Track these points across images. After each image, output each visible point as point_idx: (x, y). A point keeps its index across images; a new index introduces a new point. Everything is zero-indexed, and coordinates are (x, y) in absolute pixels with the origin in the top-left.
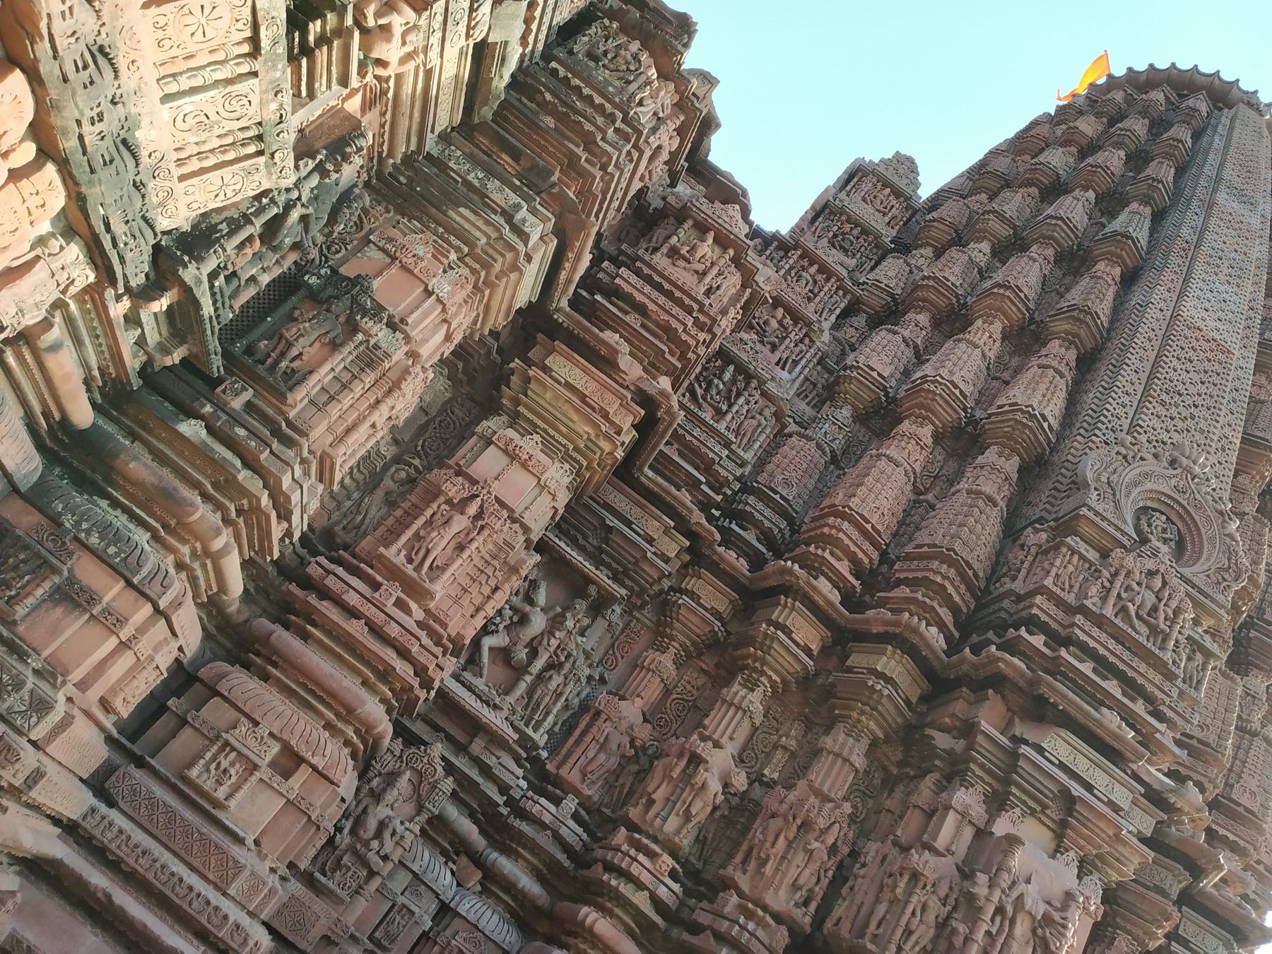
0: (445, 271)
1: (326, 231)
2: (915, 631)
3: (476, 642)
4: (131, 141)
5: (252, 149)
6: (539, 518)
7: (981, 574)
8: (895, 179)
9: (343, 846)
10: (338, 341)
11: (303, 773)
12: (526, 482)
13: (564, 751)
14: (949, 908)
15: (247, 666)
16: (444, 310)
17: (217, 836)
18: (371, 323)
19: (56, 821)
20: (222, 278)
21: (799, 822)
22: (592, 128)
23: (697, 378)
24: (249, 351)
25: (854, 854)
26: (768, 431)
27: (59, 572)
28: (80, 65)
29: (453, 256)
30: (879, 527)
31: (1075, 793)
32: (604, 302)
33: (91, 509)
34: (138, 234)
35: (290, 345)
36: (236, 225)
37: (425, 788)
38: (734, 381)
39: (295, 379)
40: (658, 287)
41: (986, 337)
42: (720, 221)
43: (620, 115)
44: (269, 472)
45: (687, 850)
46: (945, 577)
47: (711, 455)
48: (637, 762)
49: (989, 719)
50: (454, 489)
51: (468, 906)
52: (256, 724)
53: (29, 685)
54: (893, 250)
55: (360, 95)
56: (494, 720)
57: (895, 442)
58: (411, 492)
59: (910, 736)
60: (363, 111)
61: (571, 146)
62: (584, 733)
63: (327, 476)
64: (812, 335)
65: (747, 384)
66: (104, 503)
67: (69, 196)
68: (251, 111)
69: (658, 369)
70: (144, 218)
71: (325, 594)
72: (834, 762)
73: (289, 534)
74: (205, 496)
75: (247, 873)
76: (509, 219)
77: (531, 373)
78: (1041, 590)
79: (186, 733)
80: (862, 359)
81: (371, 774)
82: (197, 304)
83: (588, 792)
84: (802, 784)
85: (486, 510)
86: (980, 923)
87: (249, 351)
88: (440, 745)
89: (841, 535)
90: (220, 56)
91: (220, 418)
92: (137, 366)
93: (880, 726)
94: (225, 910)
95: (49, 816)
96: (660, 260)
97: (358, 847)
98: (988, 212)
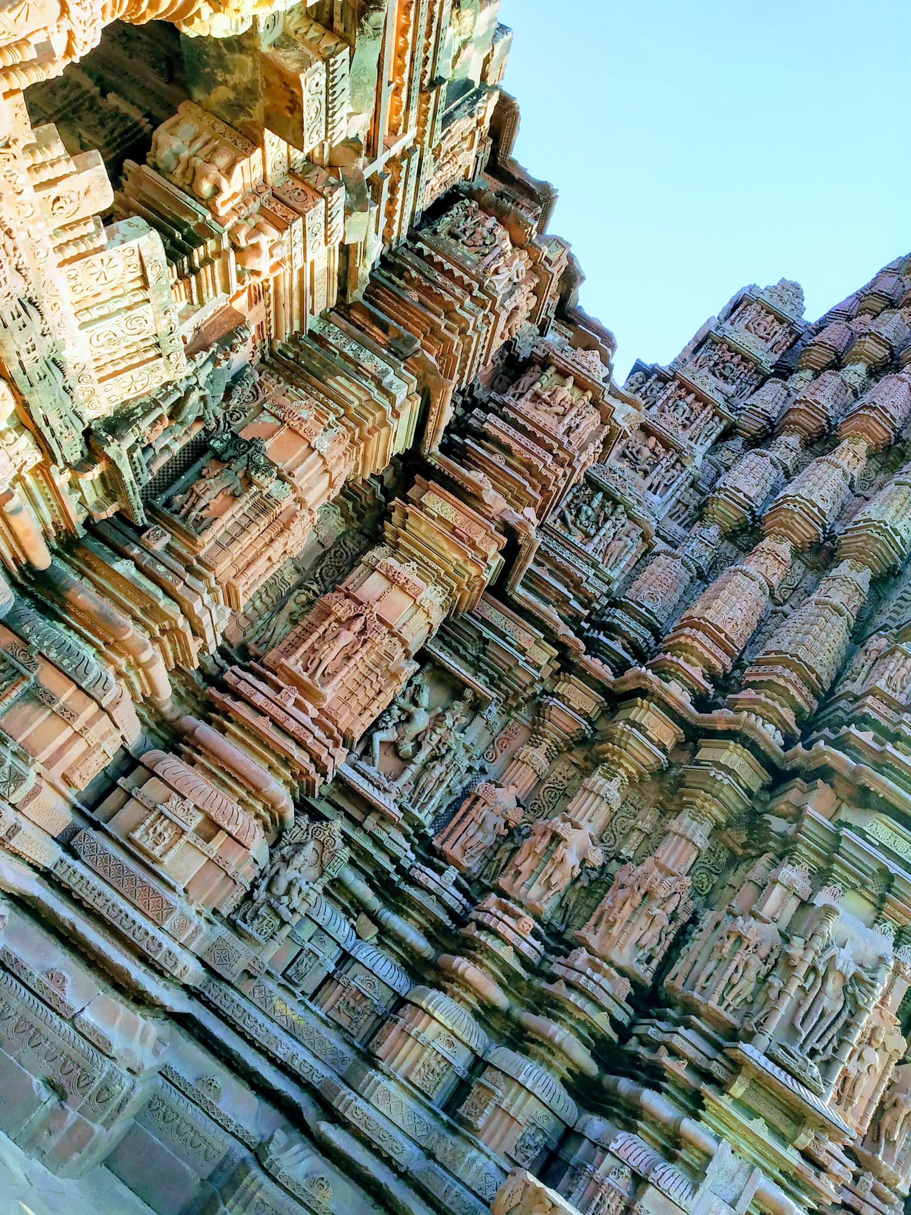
0: (325, 430)
1: (224, 405)
2: (753, 728)
3: (367, 737)
4: (58, 360)
5: (152, 353)
6: (416, 634)
7: (824, 677)
8: (779, 306)
9: (260, 901)
10: (237, 493)
11: (221, 838)
12: (407, 602)
13: (448, 830)
14: (769, 966)
15: (179, 753)
16: (325, 463)
17: (155, 884)
18: (263, 477)
19: (36, 869)
20: (139, 451)
21: (643, 891)
22: (452, 299)
23: (568, 506)
24: (168, 503)
25: (694, 920)
26: (634, 551)
27: (28, 679)
28: (16, 314)
29: (332, 417)
30: (732, 636)
31: (892, 871)
32: (473, 445)
33: (50, 631)
34: (70, 425)
35: (199, 498)
36: (148, 409)
37: (326, 856)
38: (602, 507)
39: (202, 525)
40: (522, 430)
41: (851, 456)
42: (579, 367)
43: (476, 285)
44: (184, 600)
45: (549, 915)
46: (788, 681)
47: (579, 574)
48: (512, 841)
49: (818, 805)
50: (343, 609)
51: (365, 954)
52: (184, 798)
53: (8, 763)
54: (773, 375)
55: (246, 294)
56: (382, 801)
57: (755, 558)
58: (307, 612)
59: (753, 820)
60: (250, 306)
61: (433, 316)
62: (464, 815)
63: (234, 601)
64: (683, 460)
65: (615, 508)
66: (61, 626)
67: (17, 402)
68: (148, 327)
69: (521, 502)
70: (74, 412)
71: (237, 696)
72: (678, 842)
73: (204, 649)
74: (135, 619)
75: (177, 913)
76: (379, 386)
77: (408, 510)
78: (872, 692)
79: (132, 802)
80: (729, 481)
81: (282, 843)
82: (118, 471)
83: (466, 864)
84: (649, 860)
85: (366, 624)
86: (793, 979)
87: (168, 503)
88: (339, 821)
89: (695, 643)
90: (120, 292)
91: (144, 558)
92: (81, 521)
93: (721, 811)
94: (160, 940)
95: (30, 865)
96: (524, 405)
97: (272, 901)
98: (865, 335)
